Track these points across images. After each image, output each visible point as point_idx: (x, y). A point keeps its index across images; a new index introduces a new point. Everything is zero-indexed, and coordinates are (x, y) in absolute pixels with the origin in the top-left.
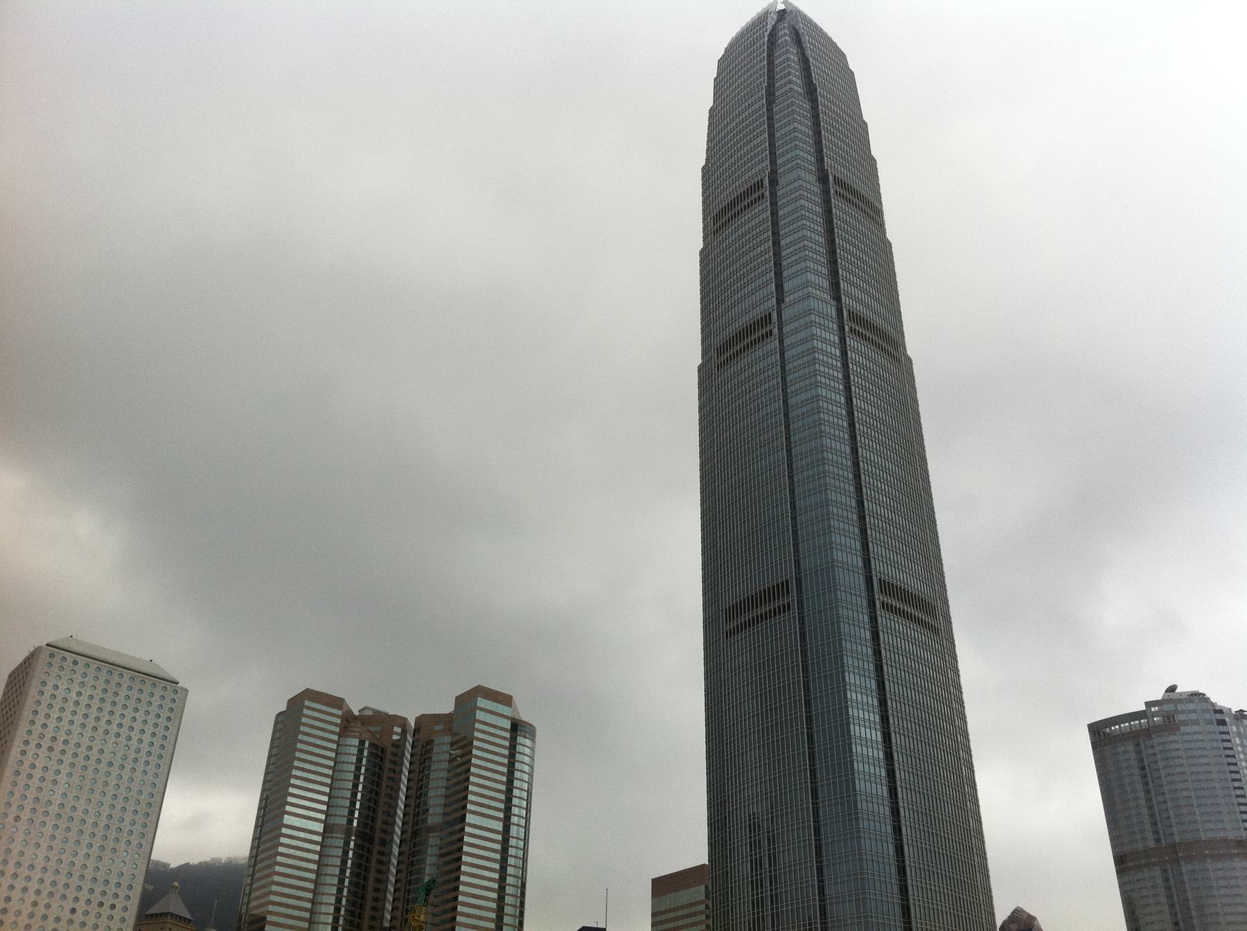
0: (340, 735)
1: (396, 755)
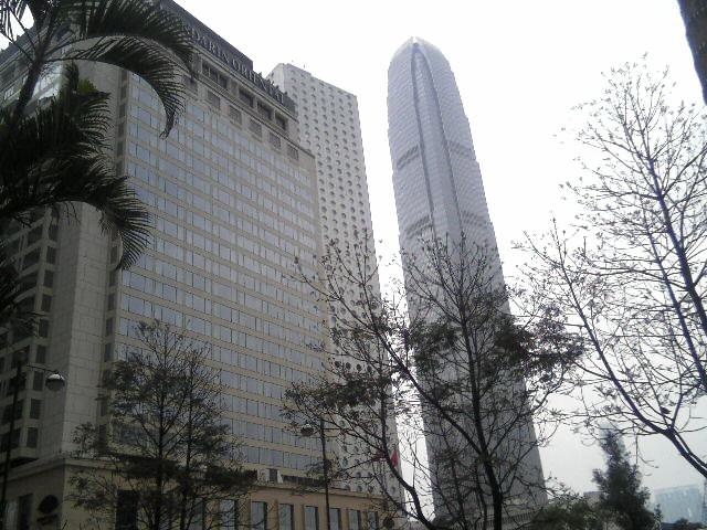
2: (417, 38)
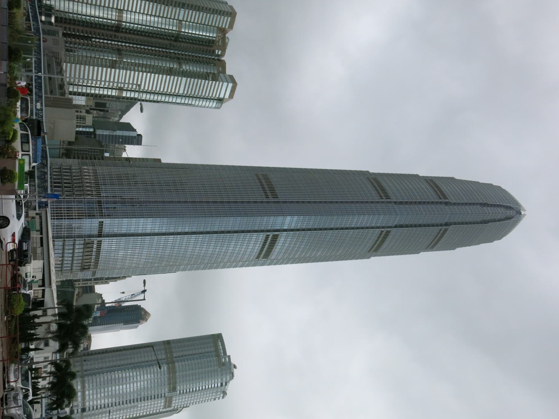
0: (218, 27)
1: (210, 52)
2: (525, 215)
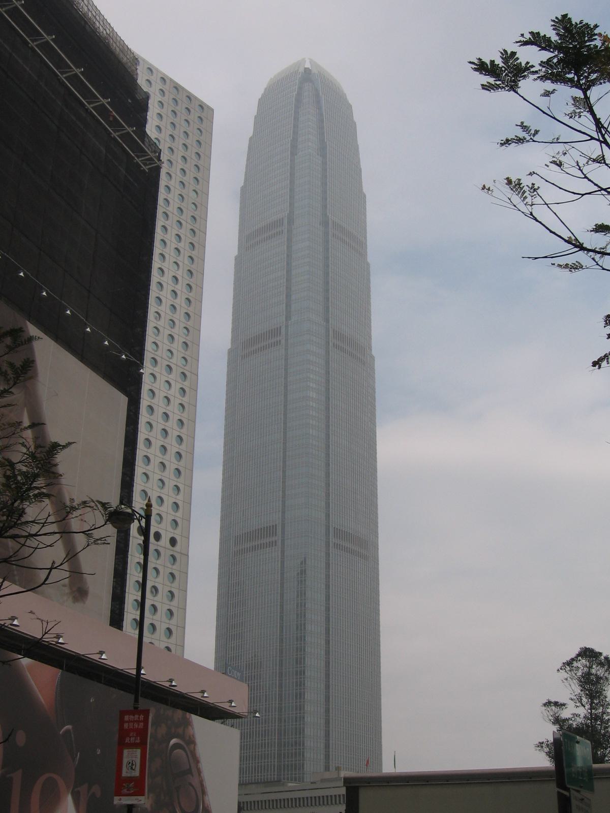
2: (311, 61)
